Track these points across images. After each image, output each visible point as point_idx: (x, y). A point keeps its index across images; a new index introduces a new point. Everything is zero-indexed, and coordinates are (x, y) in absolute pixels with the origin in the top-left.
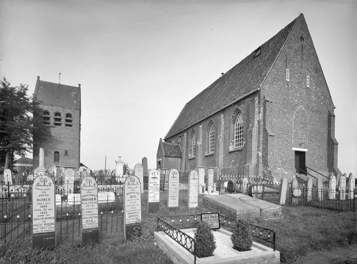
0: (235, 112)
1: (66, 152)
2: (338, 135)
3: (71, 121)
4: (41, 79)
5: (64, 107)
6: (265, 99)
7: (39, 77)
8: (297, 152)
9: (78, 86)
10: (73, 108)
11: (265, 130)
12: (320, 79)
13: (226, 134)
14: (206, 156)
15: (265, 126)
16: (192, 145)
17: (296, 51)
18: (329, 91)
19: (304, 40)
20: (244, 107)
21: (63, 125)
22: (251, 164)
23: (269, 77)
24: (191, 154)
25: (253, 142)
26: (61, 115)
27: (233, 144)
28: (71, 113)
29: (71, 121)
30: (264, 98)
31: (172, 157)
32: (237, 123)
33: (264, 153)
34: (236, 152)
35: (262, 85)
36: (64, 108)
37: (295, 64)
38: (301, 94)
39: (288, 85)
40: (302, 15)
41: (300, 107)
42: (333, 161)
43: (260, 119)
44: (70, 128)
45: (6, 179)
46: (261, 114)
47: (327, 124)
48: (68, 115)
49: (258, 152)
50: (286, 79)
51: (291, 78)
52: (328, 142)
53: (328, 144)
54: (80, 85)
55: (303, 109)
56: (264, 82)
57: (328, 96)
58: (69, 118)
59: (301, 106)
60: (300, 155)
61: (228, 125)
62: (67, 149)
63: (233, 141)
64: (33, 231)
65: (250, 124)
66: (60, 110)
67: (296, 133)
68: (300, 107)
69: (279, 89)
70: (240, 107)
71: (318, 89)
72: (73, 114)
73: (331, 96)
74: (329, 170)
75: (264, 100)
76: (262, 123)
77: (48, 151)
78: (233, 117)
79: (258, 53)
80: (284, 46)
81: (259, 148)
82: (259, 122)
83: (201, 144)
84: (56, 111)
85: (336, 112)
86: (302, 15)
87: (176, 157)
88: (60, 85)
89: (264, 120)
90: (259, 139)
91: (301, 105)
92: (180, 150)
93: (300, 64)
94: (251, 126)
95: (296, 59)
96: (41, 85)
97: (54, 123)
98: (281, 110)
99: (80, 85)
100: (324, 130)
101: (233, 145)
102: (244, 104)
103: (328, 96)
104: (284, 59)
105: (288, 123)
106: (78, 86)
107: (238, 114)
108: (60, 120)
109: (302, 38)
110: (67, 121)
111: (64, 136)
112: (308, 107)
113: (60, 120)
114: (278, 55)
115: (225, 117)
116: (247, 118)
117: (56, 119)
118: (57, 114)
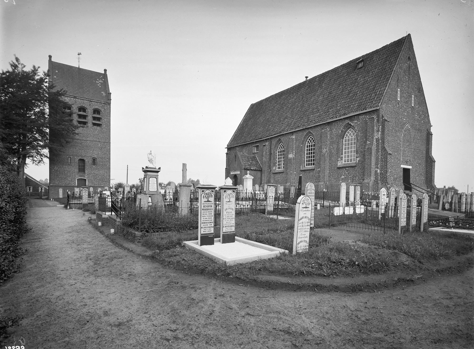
0: (345, 127)
1: (94, 160)
2: (435, 153)
3: (99, 119)
4: (53, 60)
5: (91, 100)
6: (383, 118)
7: (50, 57)
8: (404, 169)
9: (103, 72)
10: (102, 102)
11: (384, 148)
12: (422, 98)
13: (334, 149)
14: (301, 171)
15: (384, 144)
16: (276, 157)
17: (405, 72)
18: (428, 110)
19: (410, 60)
20: (359, 123)
21: (90, 125)
22: (371, 181)
23: (386, 97)
24: (276, 167)
25: (372, 159)
26: (86, 110)
27: (342, 160)
28: (100, 108)
29: (99, 119)
30: (383, 117)
31: (252, 170)
32: (346, 138)
33: (383, 171)
34: (347, 168)
35: (381, 105)
36: (91, 101)
37: (404, 84)
38: (408, 113)
39: (399, 104)
40: (409, 35)
41: (407, 126)
42: (431, 178)
43: (379, 137)
44: (98, 128)
45: (168, 196)
46: (380, 133)
47: (425, 142)
48: (96, 111)
49: (376, 169)
50: (397, 99)
51: (401, 98)
52: (427, 159)
53: (427, 161)
54: (105, 70)
55: (409, 127)
56: (382, 102)
57: (427, 115)
58: (96, 116)
59: (408, 125)
60: (406, 171)
61: (335, 139)
62: (96, 156)
63: (341, 156)
64: (417, 222)
65: (367, 141)
66: (86, 104)
67: (404, 151)
68: (407, 126)
69: (393, 108)
70: (353, 123)
71: (420, 108)
72: (102, 110)
73: (429, 115)
74: (427, 186)
75: (382, 119)
76: (380, 141)
77: (69, 158)
78: (342, 131)
79: (360, 65)
80: (396, 67)
81: (378, 165)
82: (377, 140)
83: (294, 156)
84: (80, 106)
85: (433, 130)
86: (409, 35)
87: (255, 170)
88: (79, 68)
89: (383, 139)
90: (378, 156)
91: (408, 124)
92: (258, 162)
93: (407, 84)
94: (369, 144)
95: (405, 79)
96: (53, 65)
97: (78, 121)
98: (393, 128)
99: (105, 70)
100: (423, 148)
101: (342, 161)
102: (358, 120)
103: (427, 115)
104: (396, 79)
105: (398, 141)
106: (103, 72)
107: (348, 129)
108: (85, 117)
109: (409, 58)
110: (94, 118)
111: (91, 139)
112: (412, 126)
113: (85, 117)
114: (392, 75)
115: (331, 130)
116: (362, 134)
117: (80, 116)
118: (82, 109)
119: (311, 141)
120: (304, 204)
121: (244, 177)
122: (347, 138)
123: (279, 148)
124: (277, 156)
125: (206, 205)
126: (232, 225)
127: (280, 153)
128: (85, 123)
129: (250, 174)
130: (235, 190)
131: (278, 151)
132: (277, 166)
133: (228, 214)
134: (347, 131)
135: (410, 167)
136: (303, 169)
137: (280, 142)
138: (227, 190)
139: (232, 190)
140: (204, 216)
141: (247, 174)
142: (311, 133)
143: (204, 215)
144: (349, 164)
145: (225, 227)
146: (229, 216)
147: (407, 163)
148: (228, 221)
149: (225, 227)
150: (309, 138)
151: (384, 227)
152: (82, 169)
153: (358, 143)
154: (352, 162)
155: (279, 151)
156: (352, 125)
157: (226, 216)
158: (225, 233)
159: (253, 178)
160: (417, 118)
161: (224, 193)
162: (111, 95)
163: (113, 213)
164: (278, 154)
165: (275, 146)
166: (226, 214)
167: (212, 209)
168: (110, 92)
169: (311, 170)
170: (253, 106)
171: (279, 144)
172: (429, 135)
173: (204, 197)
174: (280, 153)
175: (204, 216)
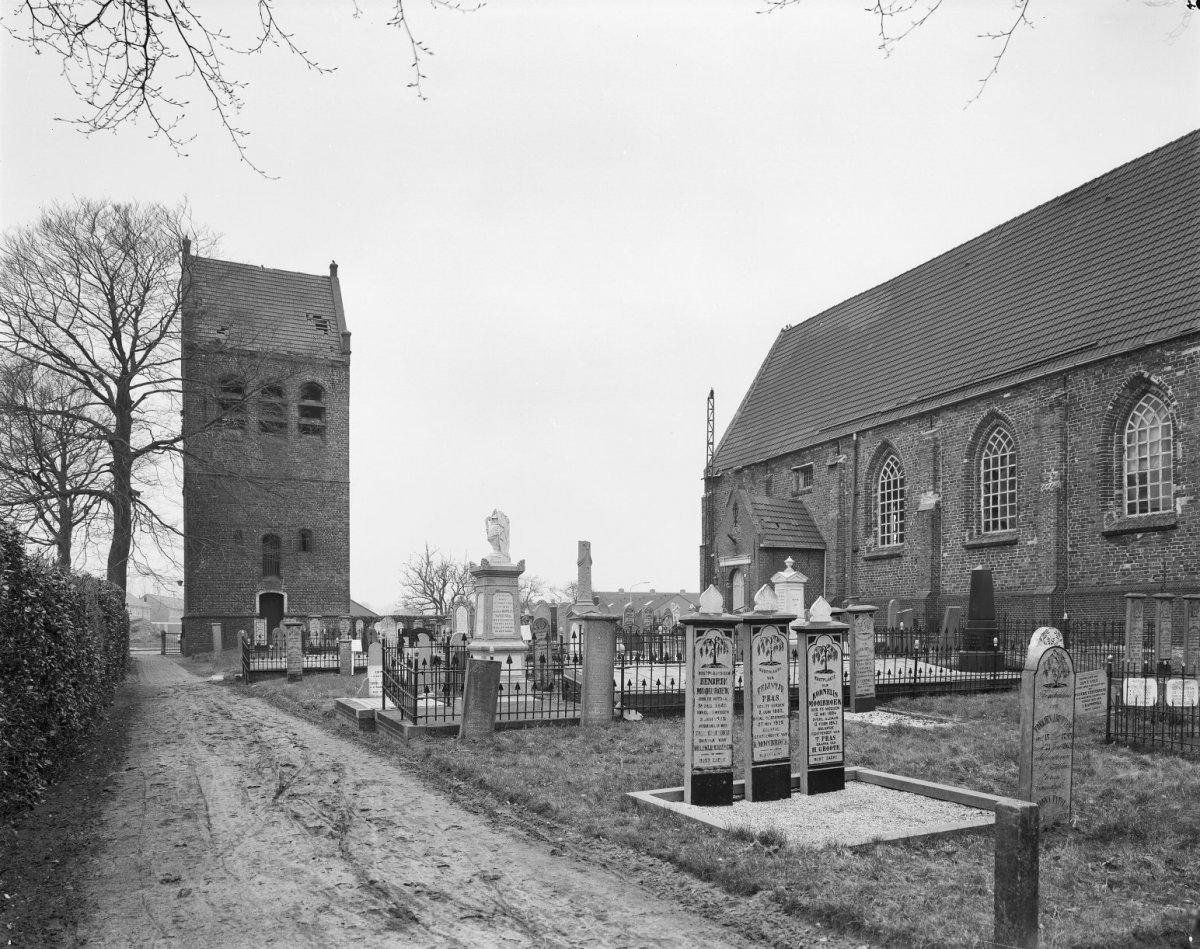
4: (199, 250)
16: (876, 505)
20: (1179, 374)
24: (876, 537)
54: (334, 267)
99: (334, 267)
106: (328, 273)
110: (307, 412)
119: (1000, 444)
120: (1050, 673)
121: (776, 576)
122: (1137, 428)
123: (885, 472)
125: (710, 676)
126: (780, 737)
127: (889, 488)
128: (282, 426)
129: (794, 568)
130: (841, 634)
131: (880, 482)
132: (880, 535)
133: (766, 702)
134: (1136, 403)
136: (974, 542)
137: (889, 454)
138: (817, 636)
139: (777, 626)
141: (783, 568)
142: (999, 417)
143: (703, 709)
144: (1159, 517)
145: (761, 744)
146: (770, 709)
148: (768, 727)
149: (761, 744)
150: (994, 434)
152: (272, 567)
153: (1180, 445)
154: (1157, 513)
155: (883, 484)
156: (1155, 381)
157: (763, 710)
158: (815, 767)
159: (805, 579)
161: (753, 637)
162: (351, 337)
163: (389, 704)
164: (880, 492)
165: (872, 468)
166: (760, 702)
167: (726, 690)
168: (349, 328)
169: (1005, 544)
170: (787, 334)
171: (886, 458)
173: (704, 653)
174: (889, 488)
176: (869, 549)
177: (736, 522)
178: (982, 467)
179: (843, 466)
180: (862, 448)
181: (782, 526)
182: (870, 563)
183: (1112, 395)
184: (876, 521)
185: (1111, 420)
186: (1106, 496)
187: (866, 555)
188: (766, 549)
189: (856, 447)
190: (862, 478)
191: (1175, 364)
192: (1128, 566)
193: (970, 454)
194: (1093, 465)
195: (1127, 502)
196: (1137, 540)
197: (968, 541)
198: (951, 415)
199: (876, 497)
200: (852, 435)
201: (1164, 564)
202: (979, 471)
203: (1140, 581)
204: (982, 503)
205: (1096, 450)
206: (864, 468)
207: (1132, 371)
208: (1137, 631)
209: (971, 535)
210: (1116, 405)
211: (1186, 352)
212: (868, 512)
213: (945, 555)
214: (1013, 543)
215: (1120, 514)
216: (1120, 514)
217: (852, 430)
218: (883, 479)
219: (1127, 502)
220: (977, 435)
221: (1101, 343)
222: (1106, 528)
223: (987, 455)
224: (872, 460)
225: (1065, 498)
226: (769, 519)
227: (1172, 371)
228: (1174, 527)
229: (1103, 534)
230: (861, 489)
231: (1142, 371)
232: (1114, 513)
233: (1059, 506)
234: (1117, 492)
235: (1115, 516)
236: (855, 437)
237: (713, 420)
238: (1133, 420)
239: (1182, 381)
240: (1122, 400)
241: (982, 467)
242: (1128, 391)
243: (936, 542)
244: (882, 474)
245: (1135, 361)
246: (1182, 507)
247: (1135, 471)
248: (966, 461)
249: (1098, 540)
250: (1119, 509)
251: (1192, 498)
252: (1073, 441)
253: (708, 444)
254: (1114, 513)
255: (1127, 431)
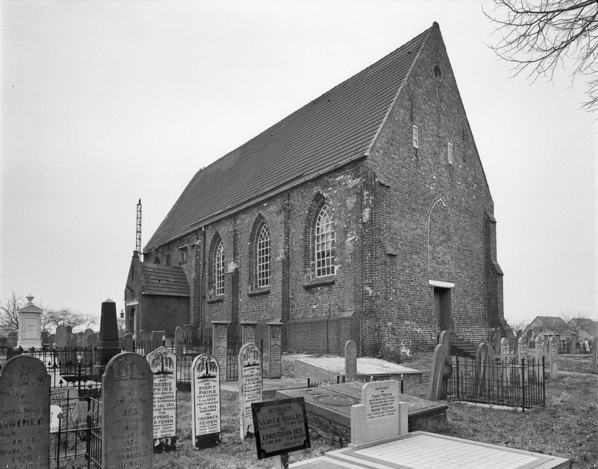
2: (503, 259)
16: (215, 270)
19: (440, 74)
20: (335, 192)
24: (214, 289)
41: (438, 201)
42: (497, 307)
53: (487, 275)
55: (444, 205)
60: (441, 292)
73: (487, 185)
75: (374, 180)
85: (497, 215)
119: (265, 234)
124: (216, 267)
132: (217, 288)
135: (450, 285)
140: (200, 404)
147: (441, 277)
151: (68, 399)
156: (325, 196)
160: (461, 188)
164: (217, 263)
165: (212, 248)
170: (201, 171)
172: (488, 226)
175: (200, 404)
176: (211, 297)
177: (133, 278)
178: (258, 248)
179: (199, 247)
180: (207, 236)
181: (162, 282)
182: (210, 305)
183: (308, 204)
184: (215, 280)
185: (308, 220)
186: (306, 265)
187: (209, 300)
188: (147, 296)
189: (204, 235)
190: (207, 254)
191: (333, 186)
192: (315, 307)
193: (251, 240)
194: (300, 246)
195: (317, 269)
196: (317, 291)
197: (250, 292)
198: (243, 216)
199: (215, 266)
200: (201, 228)
201: (329, 305)
202: (256, 250)
203: (320, 315)
204: (258, 270)
205: (302, 237)
206: (208, 248)
207: (316, 189)
208: (221, 348)
209: (252, 288)
210: (310, 211)
211: (338, 179)
212: (210, 274)
213: (241, 300)
214: (268, 292)
215: (313, 276)
216: (313, 276)
217: (202, 225)
218: (218, 255)
219: (317, 269)
220: (254, 228)
221: (305, 174)
222: (306, 284)
223: (260, 241)
224: (211, 244)
225: (288, 266)
226: (154, 277)
227: (331, 190)
228: (333, 283)
229: (304, 287)
230: (207, 261)
231: (320, 190)
232: (310, 275)
233: (283, 270)
234: (312, 262)
235: (311, 277)
236: (203, 229)
237: (140, 218)
238: (319, 220)
239: (336, 196)
240: (313, 208)
241: (258, 248)
242: (315, 202)
243: (235, 292)
244: (218, 252)
245: (317, 184)
246: (337, 271)
247: (320, 251)
248: (249, 244)
249: (302, 291)
250: (313, 273)
251: (340, 266)
252: (292, 231)
253: (137, 232)
254: (310, 275)
255: (317, 227)
